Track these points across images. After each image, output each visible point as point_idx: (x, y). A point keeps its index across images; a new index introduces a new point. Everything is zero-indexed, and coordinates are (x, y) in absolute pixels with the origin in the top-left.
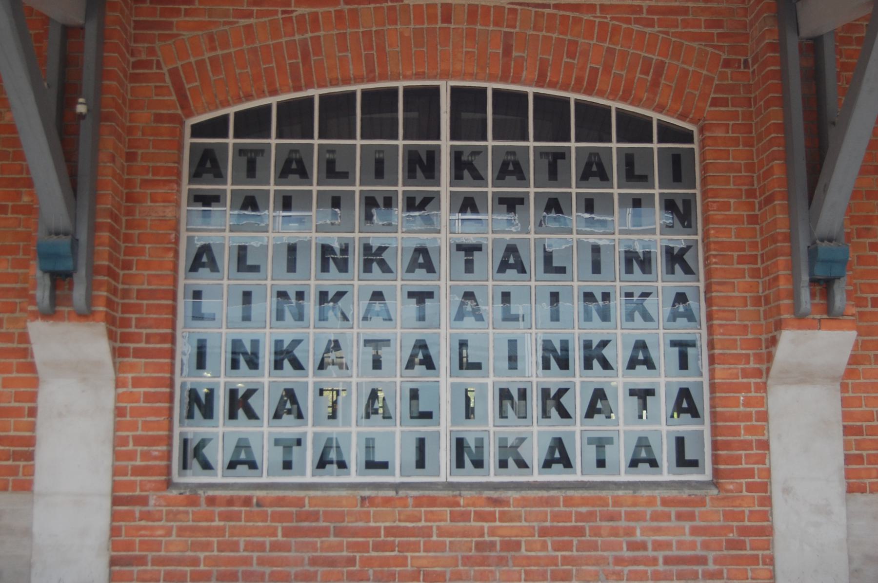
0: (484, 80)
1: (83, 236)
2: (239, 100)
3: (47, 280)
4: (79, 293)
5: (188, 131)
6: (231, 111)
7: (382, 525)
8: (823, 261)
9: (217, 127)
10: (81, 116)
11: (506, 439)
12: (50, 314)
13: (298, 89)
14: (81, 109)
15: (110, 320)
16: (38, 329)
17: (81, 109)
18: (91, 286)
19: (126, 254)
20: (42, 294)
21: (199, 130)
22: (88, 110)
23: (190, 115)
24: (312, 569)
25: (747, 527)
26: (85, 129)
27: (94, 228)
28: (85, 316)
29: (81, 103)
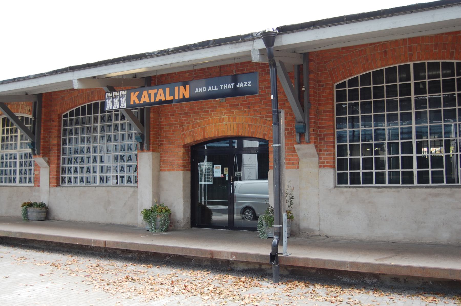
0: (424, 60)
1: (306, 122)
2: (348, 77)
3: (298, 135)
4: (306, 137)
5: (335, 87)
6: (347, 80)
7: (198, 128)
8: (213, 167)
9: (343, 85)
10: (304, 91)
11: (131, 140)
12: (300, 143)
13: (365, 71)
14: (303, 89)
15: (315, 143)
16: (296, 146)
17: (303, 89)
18: (309, 136)
19: (320, 124)
20: (297, 138)
21: (338, 87)
22: (305, 89)
23: (335, 83)
24: (198, 111)
25: (61, 119)
26: (305, 94)
27: (309, 119)
28: (309, 142)
29: (304, 88)
